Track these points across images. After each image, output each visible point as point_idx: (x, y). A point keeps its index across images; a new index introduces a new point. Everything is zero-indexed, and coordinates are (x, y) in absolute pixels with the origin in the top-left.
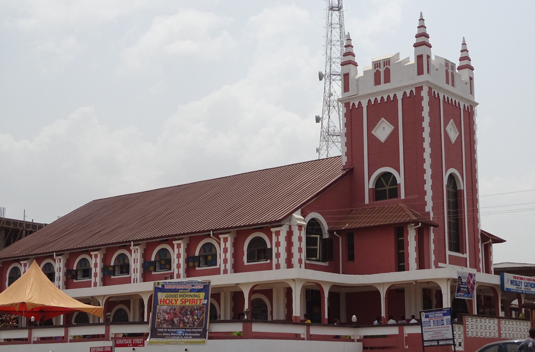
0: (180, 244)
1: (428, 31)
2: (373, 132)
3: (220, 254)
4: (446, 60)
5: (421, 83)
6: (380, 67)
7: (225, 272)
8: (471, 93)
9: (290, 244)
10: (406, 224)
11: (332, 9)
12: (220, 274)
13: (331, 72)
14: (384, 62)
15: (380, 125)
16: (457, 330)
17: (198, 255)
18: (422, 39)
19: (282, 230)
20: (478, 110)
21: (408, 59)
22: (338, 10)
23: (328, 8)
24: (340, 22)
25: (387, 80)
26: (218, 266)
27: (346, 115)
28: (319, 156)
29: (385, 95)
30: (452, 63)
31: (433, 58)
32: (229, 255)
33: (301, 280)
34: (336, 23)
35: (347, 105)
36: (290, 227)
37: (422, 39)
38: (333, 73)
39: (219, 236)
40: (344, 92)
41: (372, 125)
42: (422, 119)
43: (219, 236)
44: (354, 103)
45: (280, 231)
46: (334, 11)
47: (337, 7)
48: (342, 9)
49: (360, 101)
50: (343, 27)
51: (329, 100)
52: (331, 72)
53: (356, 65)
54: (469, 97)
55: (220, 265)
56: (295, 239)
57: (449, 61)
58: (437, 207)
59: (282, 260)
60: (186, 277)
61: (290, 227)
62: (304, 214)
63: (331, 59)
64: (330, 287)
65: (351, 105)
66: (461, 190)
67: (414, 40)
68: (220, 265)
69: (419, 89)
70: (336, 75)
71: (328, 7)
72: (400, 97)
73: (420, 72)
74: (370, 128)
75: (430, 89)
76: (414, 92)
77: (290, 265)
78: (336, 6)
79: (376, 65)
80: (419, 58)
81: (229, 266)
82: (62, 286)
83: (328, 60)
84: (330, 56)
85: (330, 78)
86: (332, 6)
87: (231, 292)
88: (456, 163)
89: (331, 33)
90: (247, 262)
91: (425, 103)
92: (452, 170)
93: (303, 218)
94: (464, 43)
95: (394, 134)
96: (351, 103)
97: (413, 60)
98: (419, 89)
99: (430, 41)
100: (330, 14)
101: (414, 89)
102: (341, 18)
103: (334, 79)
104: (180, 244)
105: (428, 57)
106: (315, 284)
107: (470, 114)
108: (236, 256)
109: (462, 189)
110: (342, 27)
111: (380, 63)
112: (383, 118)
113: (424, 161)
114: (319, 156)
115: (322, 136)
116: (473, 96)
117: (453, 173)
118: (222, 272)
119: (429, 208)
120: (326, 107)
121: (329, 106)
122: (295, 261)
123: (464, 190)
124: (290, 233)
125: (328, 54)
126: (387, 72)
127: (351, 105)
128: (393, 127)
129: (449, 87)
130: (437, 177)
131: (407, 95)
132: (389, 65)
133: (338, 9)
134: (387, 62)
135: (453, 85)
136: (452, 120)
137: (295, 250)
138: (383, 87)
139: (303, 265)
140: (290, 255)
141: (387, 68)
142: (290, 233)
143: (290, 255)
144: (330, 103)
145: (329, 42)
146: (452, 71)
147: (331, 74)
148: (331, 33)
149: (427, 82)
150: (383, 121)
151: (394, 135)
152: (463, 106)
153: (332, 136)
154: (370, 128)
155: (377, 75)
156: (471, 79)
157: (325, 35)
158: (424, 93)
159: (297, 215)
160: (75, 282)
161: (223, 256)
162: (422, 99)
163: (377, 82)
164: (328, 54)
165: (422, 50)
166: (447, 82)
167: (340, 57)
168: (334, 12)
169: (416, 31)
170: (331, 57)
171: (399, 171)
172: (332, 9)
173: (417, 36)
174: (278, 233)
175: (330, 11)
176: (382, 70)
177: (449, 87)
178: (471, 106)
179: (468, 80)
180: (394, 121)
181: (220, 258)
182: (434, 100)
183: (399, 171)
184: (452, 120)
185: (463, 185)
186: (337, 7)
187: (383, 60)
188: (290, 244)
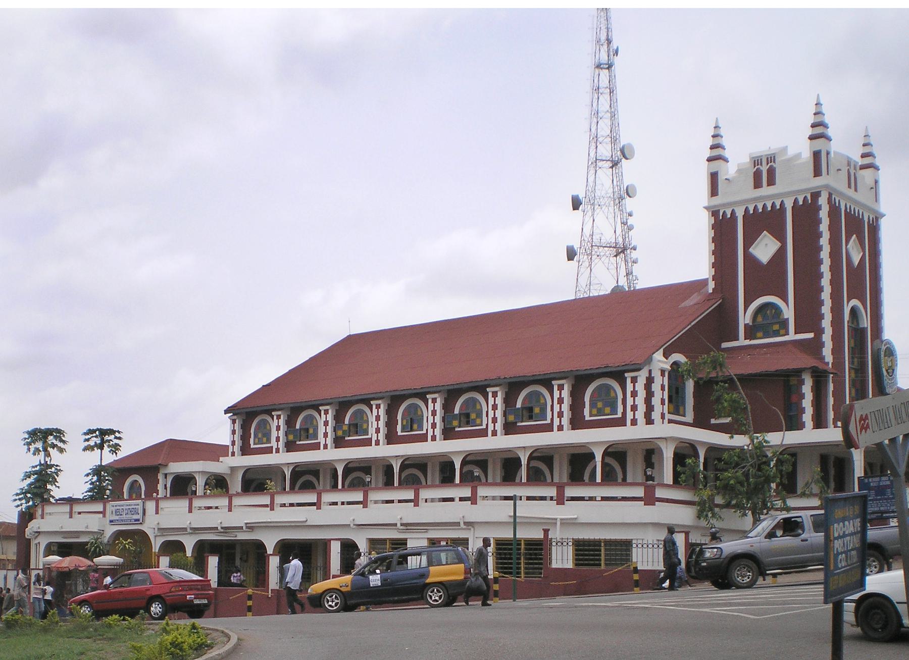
0: (497, 392)
1: (827, 119)
2: (751, 250)
3: (427, 417)
4: (848, 157)
5: (818, 187)
6: (761, 165)
7: (434, 438)
8: (876, 201)
9: (650, 394)
10: (798, 372)
11: (599, 66)
12: (636, 425)
13: (596, 156)
14: (768, 158)
15: (761, 240)
16: (872, 509)
17: (520, 407)
18: (819, 130)
19: (640, 376)
20: (884, 224)
21: (798, 156)
22: (608, 68)
23: (593, 66)
24: (610, 85)
25: (771, 182)
26: (369, 436)
27: (713, 227)
28: (578, 276)
29: (770, 201)
30: (854, 161)
31: (832, 155)
32: (382, 424)
33: (673, 439)
34: (605, 86)
35: (715, 214)
36: (650, 371)
37: (819, 130)
38: (600, 158)
39: (552, 382)
40: (711, 197)
41: (749, 241)
42: (820, 235)
43: (552, 382)
44: (724, 212)
45: (637, 377)
46: (602, 69)
47: (606, 64)
48: (613, 67)
49: (735, 208)
50: (614, 92)
51: (593, 196)
52: (596, 156)
53: (726, 160)
54: (873, 206)
55: (427, 430)
56: (656, 387)
57: (851, 159)
58: (837, 351)
59: (640, 414)
60: (386, 443)
61: (650, 371)
62: (666, 355)
63: (597, 137)
64: (705, 450)
65: (721, 214)
66: (864, 328)
67: (810, 132)
68: (427, 430)
69: (816, 195)
70: (604, 160)
71: (594, 64)
72: (789, 205)
73: (817, 172)
74: (748, 244)
75: (830, 195)
76: (809, 198)
77: (649, 421)
78: (605, 62)
79: (756, 161)
80: (817, 155)
81: (381, 436)
82: (331, 444)
83: (593, 138)
84: (595, 135)
85: (596, 165)
86: (599, 62)
87: (568, 454)
88: (856, 292)
89: (598, 101)
90: (402, 432)
91: (824, 214)
92: (855, 302)
93: (665, 360)
94: (867, 134)
95: (781, 253)
96: (721, 210)
97: (807, 156)
98: (816, 195)
99: (830, 132)
100: (596, 74)
101: (809, 194)
102: (612, 79)
103: (600, 166)
104: (497, 392)
105: (828, 153)
106: (688, 445)
107: (874, 229)
108: (391, 424)
109: (866, 326)
110: (613, 91)
111: (761, 159)
112: (765, 232)
113: (821, 289)
114: (578, 276)
115: (583, 247)
116: (879, 204)
117: (855, 305)
118: (555, 428)
119: (827, 352)
120: (589, 206)
121: (593, 204)
122: (656, 415)
123: (867, 328)
124: (650, 380)
125: (593, 130)
126: (771, 172)
127: (721, 214)
128: (779, 244)
129: (850, 193)
130: (837, 310)
131: (800, 202)
132: (774, 162)
133: (607, 66)
134: (771, 159)
135: (856, 190)
136: (855, 235)
137: (656, 401)
138: (766, 191)
139: (666, 421)
140: (650, 408)
141: (771, 166)
142: (650, 380)
143: (650, 408)
144: (594, 200)
145: (594, 114)
146: (849, 167)
147: (596, 159)
148: (598, 101)
149: (827, 187)
150: (765, 235)
151: (780, 255)
152: (868, 217)
153: (597, 247)
154: (748, 244)
155: (757, 176)
156: (876, 182)
157: (589, 102)
158: (823, 201)
159: (658, 356)
160: (400, 436)
161: (375, 423)
162: (819, 208)
163: (757, 184)
164: (593, 130)
165: (819, 144)
166: (849, 187)
167: (610, 135)
168: (602, 72)
169: (811, 120)
170: (597, 135)
171: (786, 301)
172: (599, 66)
173: (813, 126)
174: (634, 380)
175: (597, 70)
176: (764, 169)
177: (850, 193)
178: (877, 219)
179: (873, 185)
180: (780, 236)
181: (427, 422)
182: (834, 211)
183: (786, 301)
184: (855, 235)
185: (866, 322)
186: (606, 64)
187: (766, 155)
188: (650, 394)
